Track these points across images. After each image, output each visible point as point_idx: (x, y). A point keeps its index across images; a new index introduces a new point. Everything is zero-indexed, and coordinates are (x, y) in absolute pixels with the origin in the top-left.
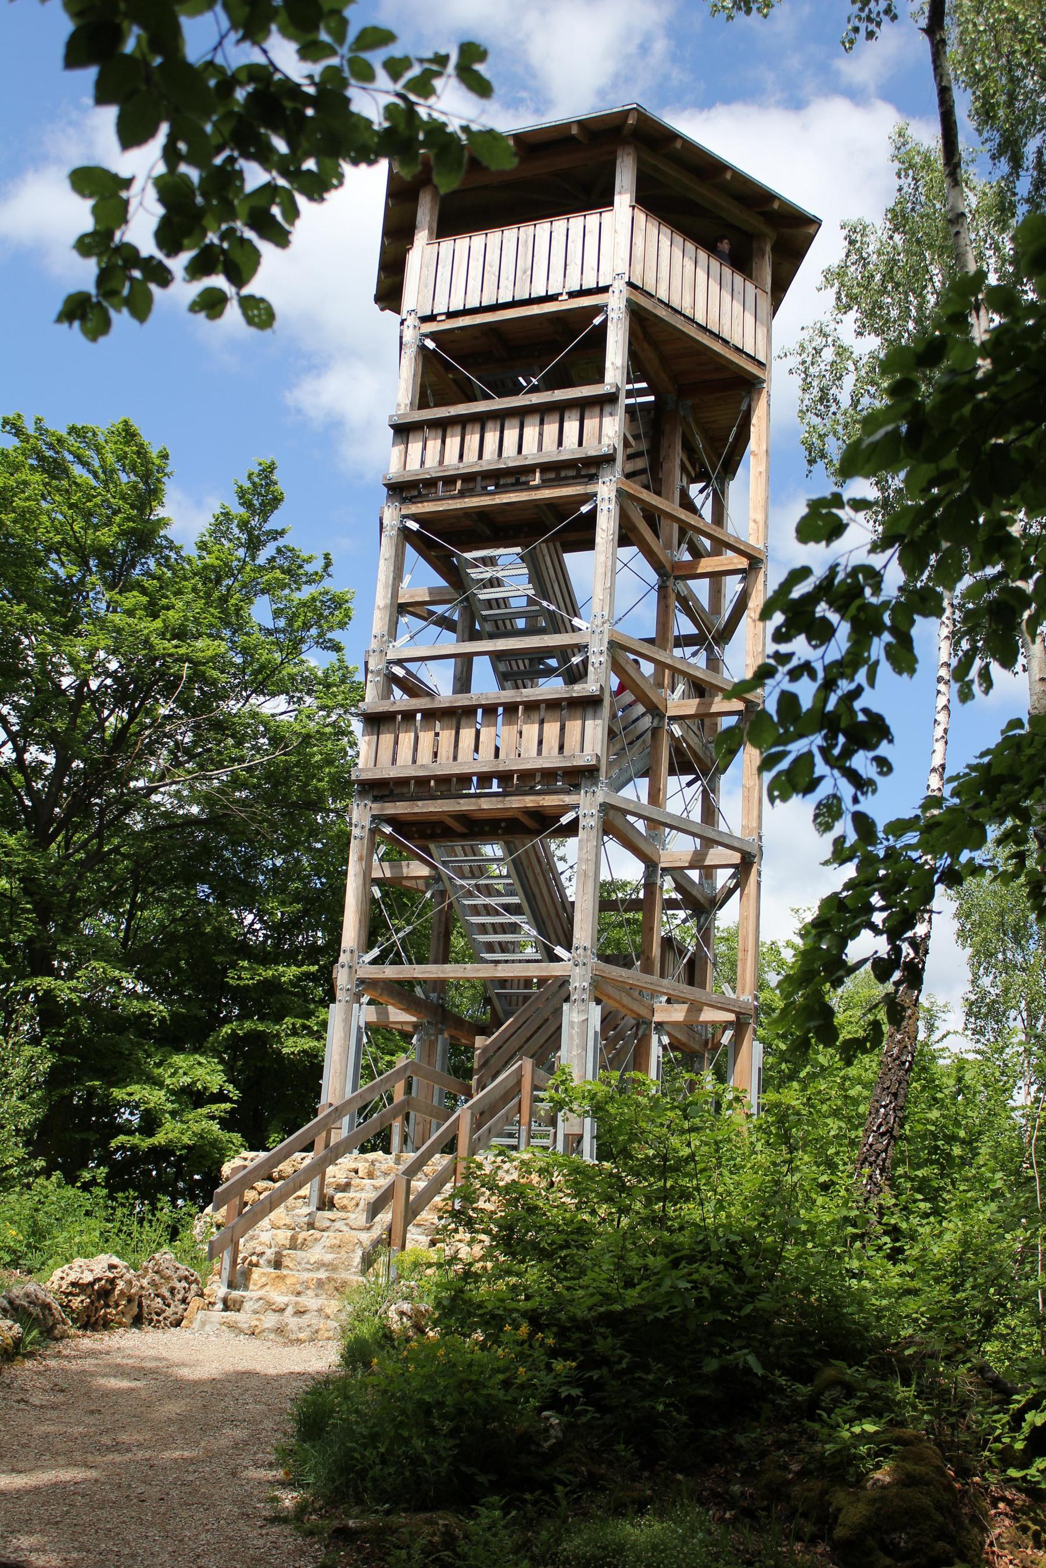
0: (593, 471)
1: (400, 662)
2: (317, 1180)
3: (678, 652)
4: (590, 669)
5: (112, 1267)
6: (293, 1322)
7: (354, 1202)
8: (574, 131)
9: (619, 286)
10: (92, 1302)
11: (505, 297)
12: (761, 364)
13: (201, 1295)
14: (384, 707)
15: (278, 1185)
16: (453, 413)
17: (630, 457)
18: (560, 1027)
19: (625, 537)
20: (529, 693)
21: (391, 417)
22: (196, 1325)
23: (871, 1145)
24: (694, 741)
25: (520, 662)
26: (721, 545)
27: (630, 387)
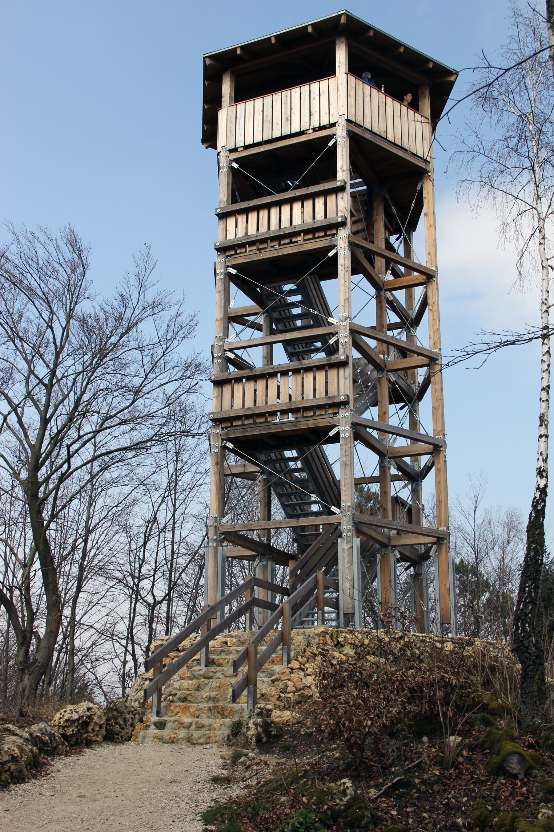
0: (334, 232)
1: (231, 350)
2: (204, 650)
3: (390, 333)
4: (340, 346)
5: (89, 709)
6: (196, 734)
7: (226, 661)
8: (310, 29)
9: (342, 123)
10: (79, 730)
11: (277, 134)
12: (426, 161)
13: (141, 721)
14: (224, 376)
15: (182, 654)
16: (251, 205)
17: (354, 223)
18: (337, 552)
19: (356, 268)
20: (306, 363)
21: (216, 209)
22: (140, 739)
23: (522, 610)
24: (402, 383)
25: (300, 345)
26: (411, 268)
27: (352, 182)
